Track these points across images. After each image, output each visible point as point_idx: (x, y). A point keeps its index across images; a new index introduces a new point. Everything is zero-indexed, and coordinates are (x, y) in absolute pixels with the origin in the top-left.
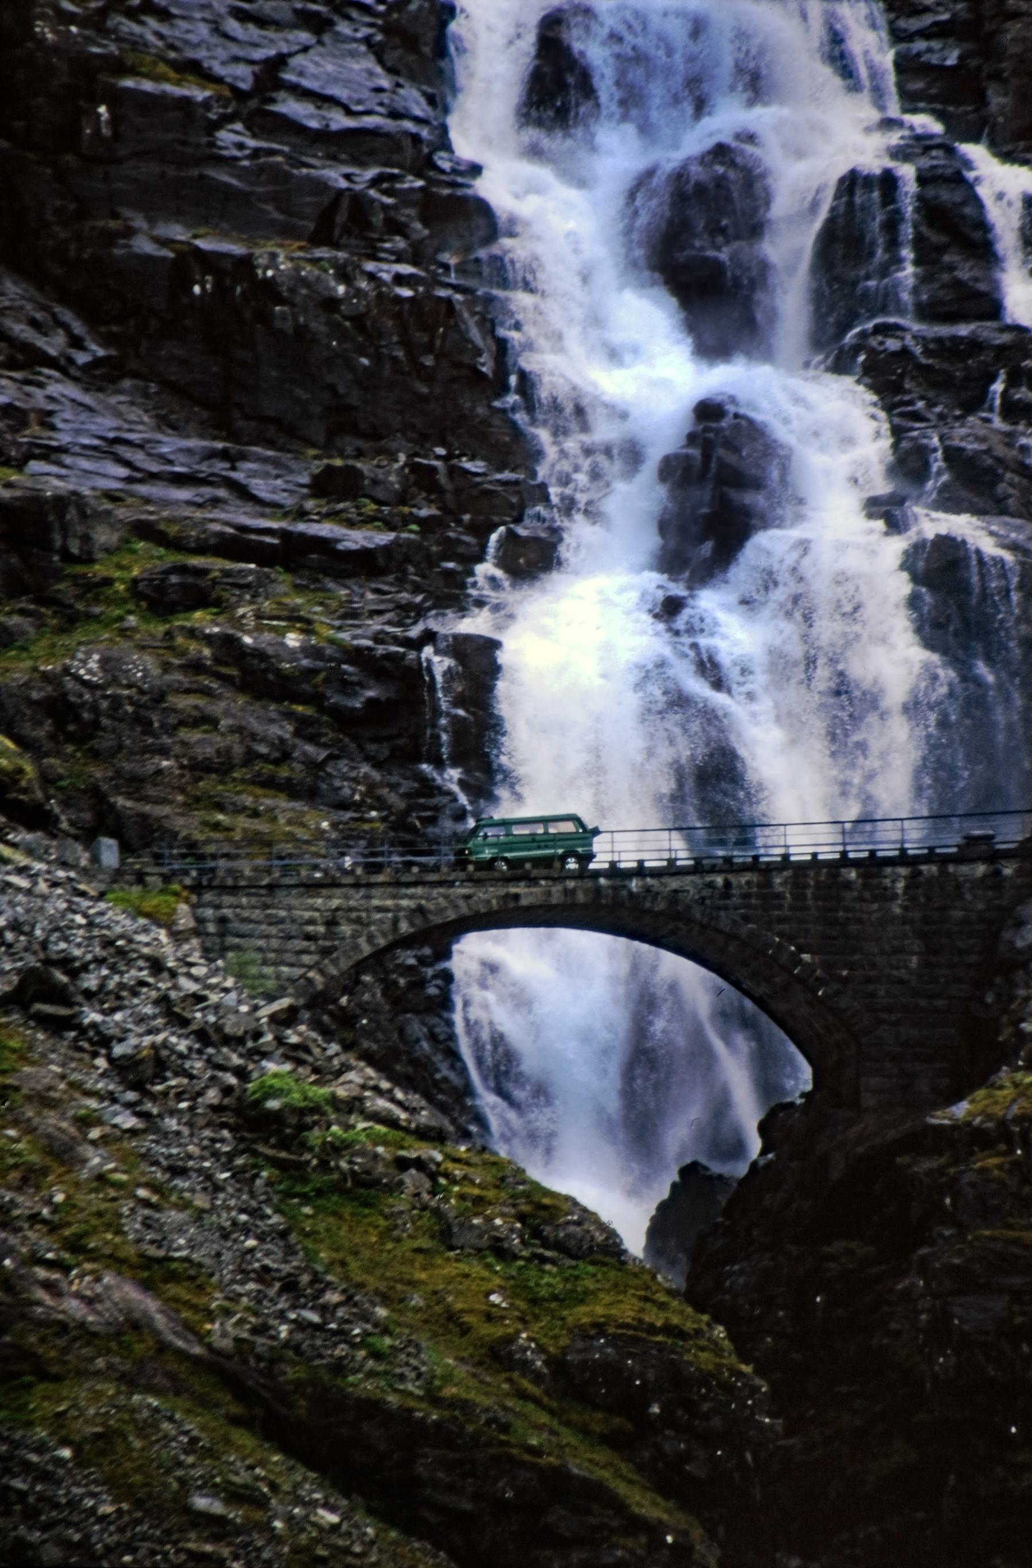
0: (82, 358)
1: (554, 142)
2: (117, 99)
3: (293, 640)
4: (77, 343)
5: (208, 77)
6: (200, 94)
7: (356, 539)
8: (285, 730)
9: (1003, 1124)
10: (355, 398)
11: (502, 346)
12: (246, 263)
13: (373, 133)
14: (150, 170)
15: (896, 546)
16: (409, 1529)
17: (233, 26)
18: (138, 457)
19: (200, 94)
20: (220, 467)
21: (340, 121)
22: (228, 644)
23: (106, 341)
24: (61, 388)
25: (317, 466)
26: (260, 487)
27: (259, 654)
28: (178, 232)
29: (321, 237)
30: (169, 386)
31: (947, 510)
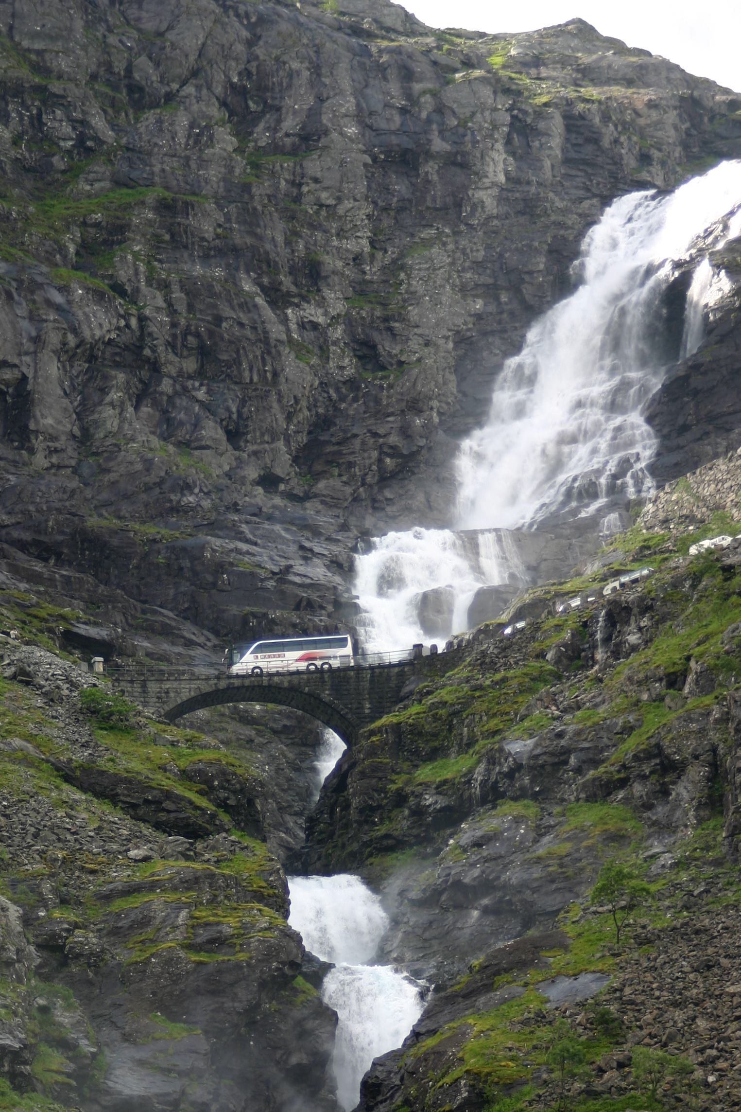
21: (308, 581)
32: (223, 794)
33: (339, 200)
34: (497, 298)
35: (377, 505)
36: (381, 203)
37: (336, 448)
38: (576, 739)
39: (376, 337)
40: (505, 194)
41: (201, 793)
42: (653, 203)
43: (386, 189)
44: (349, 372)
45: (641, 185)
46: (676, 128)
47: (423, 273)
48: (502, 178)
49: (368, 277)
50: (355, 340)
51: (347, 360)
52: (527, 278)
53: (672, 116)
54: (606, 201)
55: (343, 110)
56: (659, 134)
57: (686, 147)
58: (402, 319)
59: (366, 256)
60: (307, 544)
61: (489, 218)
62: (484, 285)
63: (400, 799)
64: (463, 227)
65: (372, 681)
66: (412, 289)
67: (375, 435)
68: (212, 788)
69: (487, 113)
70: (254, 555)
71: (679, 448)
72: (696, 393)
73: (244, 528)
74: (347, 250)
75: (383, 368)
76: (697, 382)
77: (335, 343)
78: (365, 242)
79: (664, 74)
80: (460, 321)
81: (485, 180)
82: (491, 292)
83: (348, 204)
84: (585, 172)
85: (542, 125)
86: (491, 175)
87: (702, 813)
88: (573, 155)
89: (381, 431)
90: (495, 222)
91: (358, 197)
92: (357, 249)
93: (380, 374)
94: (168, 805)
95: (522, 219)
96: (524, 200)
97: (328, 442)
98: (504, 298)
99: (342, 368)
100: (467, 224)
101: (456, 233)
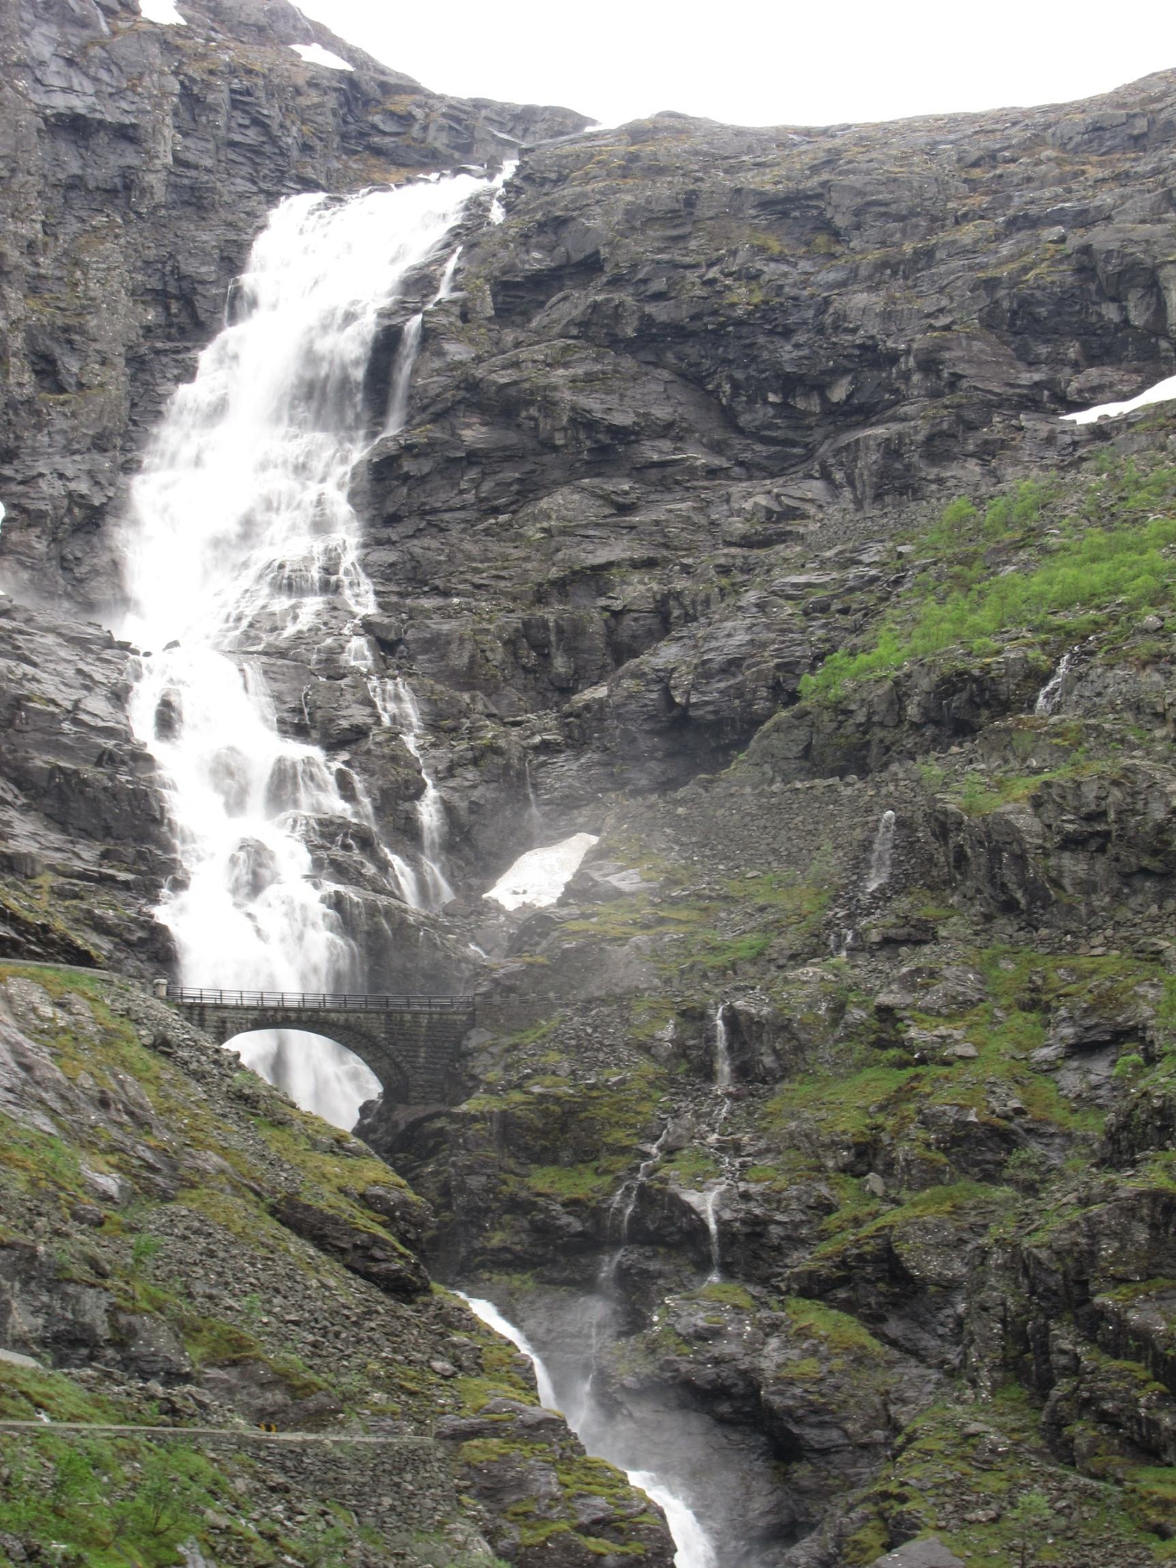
0: (19, 803)
1: (167, 737)
2: (28, 710)
3: (111, 912)
4: (16, 797)
5: (57, 705)
6: (57, 711)
7: (123, 876)
8: (111, 946)
9: (491, 1113)
10: (113, 824)
11: (162, 808)
12: (76, 772)
13: (112, 729)
14: (39, 736)
15: (318, 894)
16: (325, 1250)
17: (62, 688)
18: (42, 840)
19: (57, 711)
20: (70, 846)
21: (101, 724)
22: (89, 912)
23: (26, 796)
24: (13, 813)
25: (102, 848)
26: (85, 855)
27: (101, 917)
28: (51, 759)
29: (98, 764)
30: (48, 816)
31: (70, 962)
32: (402, 1225)
33: (13, 171)
34: (167, 308)
35: (80, 571)
36: (52, 179)
37: (20, 488)
38: (127, 758)
39: (57, 351)
40: (173, 178)
41: (383, 1224)
42: (327, 213)
43: (58, 163)
44: (28, 391)
45: (309, 185)
46: (335, 114)
47: (100, 274)
48: (169, 160)
49: (43, 271)
50: (35, 353)
51: (26, 376)
52: (199, 288)
53: (332, 101)
54: (272, 198)
55: (14, 58)
56: (320, 119)
57: (344, 137)
58: (82, 331)
59: (40, 244)
60: (82, 666)
61: (157, 207)
62: (153, 290)
63: (516, 1206)
64: (132, 216)
65: (429, 1028)
66: (92, 294)
67: (61, 476)
68: (393, 1218)
69: (155, 77)
70: (38, 681)
71: (390, 542)
72: (406, 478)
73: (20, 640)
74: (23, 237)
75: (61, 389)
76: (408, 466)
77: (14, 355)
78: (38, 226)
79: (292, 22)
80: (133, 336)
81: (157, 161)
82: (160, 297)
83: (21, 177)
84: (250, 159)
85: (211, 98)
86: (161, 155)
87: (995, 1375)
88: (238, 138)
89: (69, 473)
90: (163, 212)
91: (33, 170)
92: (31, 235)
93: (62, 397)
94: (378, 1254)
95: (189, 210)
96: (192, 189)
97: (9, 479)
98: (174, 310)
99: (20, 385)
100: (136, 213)
101: (127, 222)
